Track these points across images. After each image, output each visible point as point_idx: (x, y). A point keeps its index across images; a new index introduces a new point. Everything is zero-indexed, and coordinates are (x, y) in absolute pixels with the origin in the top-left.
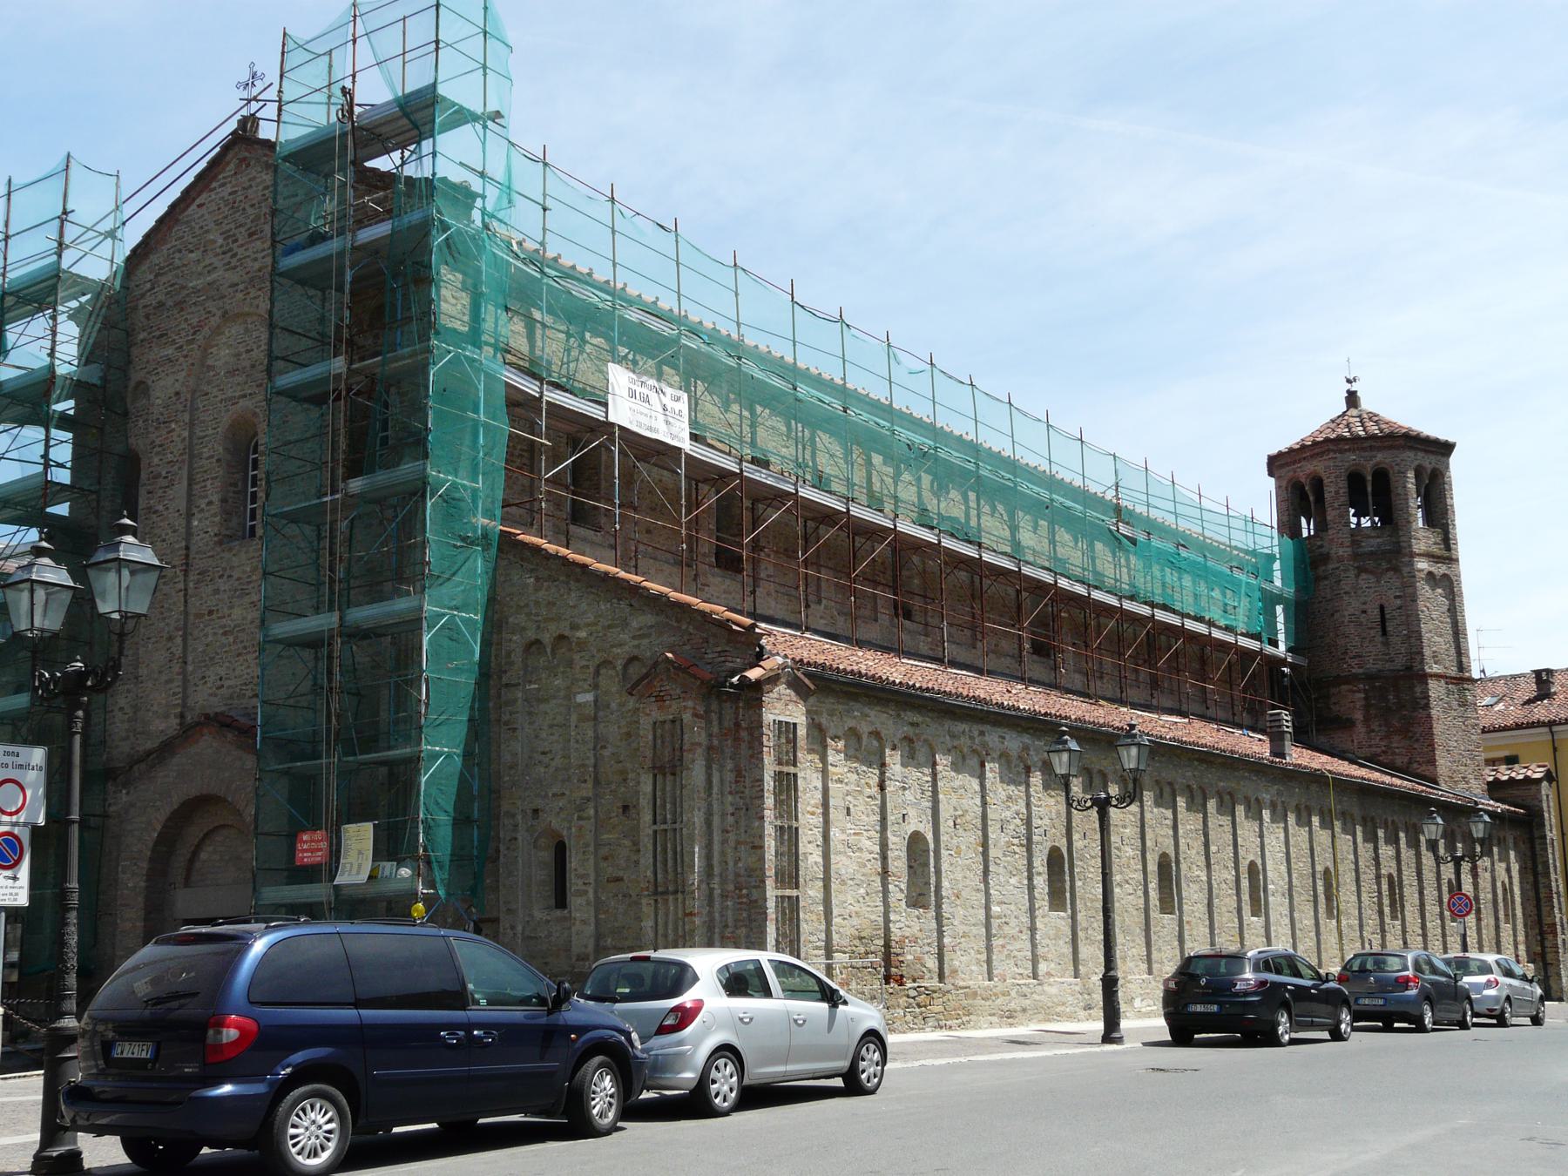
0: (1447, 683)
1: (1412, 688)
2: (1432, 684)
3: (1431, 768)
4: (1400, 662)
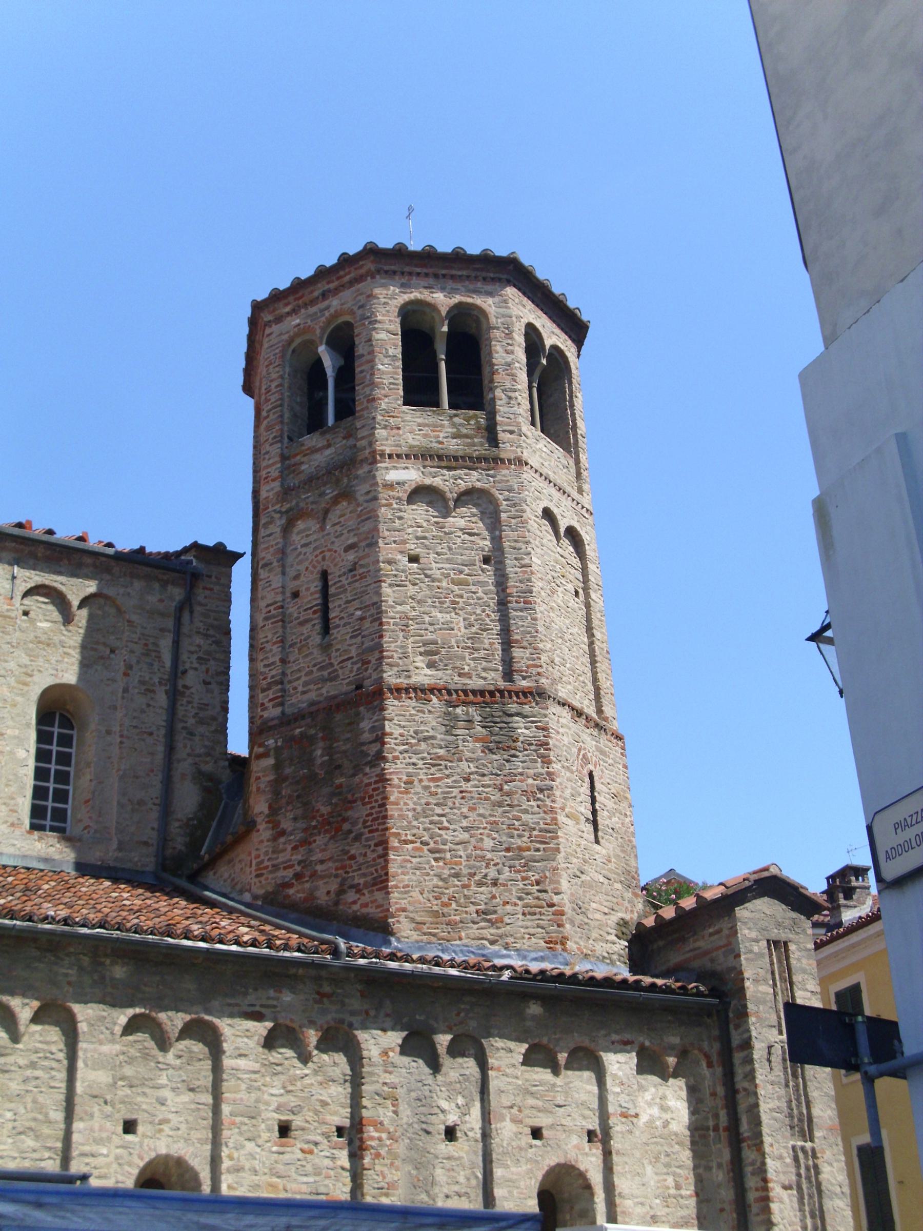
0: (449, 704)
1: (353, 724)
2: (392, 705)
3: (379, 895)
4: (347, 674)
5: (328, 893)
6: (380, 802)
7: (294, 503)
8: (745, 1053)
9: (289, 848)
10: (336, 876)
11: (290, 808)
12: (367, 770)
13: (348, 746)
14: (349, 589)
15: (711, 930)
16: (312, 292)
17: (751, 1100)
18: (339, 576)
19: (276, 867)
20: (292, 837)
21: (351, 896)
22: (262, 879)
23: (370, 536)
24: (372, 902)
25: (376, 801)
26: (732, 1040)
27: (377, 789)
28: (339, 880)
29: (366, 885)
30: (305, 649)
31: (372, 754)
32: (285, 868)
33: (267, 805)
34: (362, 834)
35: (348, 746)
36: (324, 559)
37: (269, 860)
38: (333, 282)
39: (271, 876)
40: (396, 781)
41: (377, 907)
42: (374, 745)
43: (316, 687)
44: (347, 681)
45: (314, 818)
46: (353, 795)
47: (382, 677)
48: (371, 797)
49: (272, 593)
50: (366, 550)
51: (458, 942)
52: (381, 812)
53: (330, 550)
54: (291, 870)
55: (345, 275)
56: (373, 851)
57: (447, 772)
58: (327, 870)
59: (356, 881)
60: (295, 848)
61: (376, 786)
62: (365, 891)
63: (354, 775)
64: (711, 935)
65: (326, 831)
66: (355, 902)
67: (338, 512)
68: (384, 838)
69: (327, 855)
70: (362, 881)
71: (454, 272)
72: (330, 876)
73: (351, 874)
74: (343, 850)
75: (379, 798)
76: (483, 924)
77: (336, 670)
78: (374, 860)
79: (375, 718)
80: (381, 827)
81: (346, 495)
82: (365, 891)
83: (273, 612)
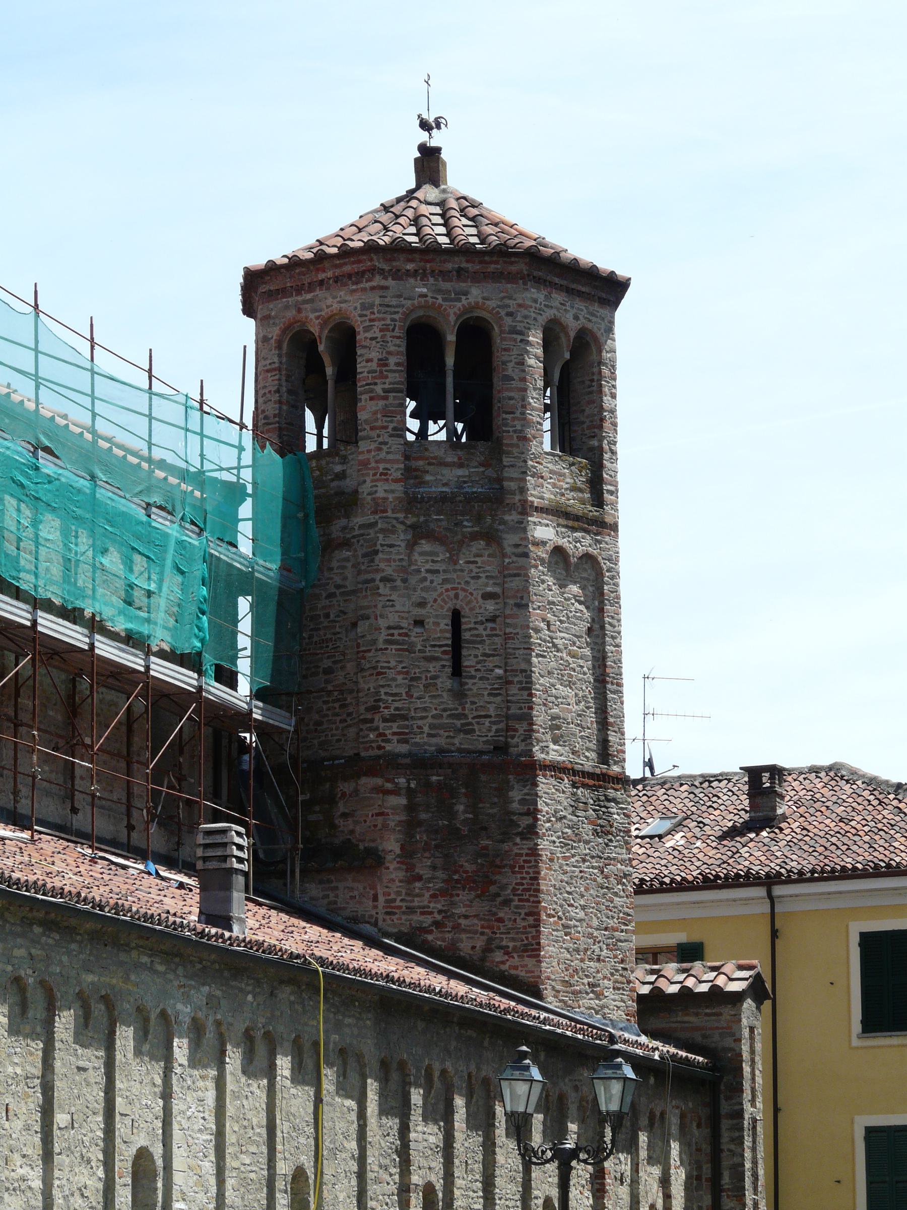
1: (502, 791)
3: (530, 962)
5: (473, 948)
6: (532, 875)
7: (422, 519)
8: (735, 1121)
9: (427, 895)
10: (482, 934)
11: (427, 854)
12: (518, 840)
13: (495, 810)
14: (488, 642)
15: (708, 1011)
16: (445, 261)
17: (736, 1160)
18: (476, 623)
19: (411, 910)
20: (431, 885)
21: (498, 956)
22: (394, 917)
23: (519, 595)
24: (522, 966)
25: (528, 873)
26: (721, 1108)
27: (530, 862)
28: (485, 938)
29: (515, 949)
30: (431, 688)
31: (522, 826)
32: (422, 913)
33: (399, 844)
34: (511, 901)
35: (495, 810)
36: (456, 596)
37: (402, 900)
38: (474, 262)
39: (404, 917)
40: (544, 858)
41: (527, 972)
42: (525, 817)
43: (446, 734)
44: (485, 739)
45: (456, 872)
46: (502, 860)
47: (531, 750)
48: (521, 867)
49: (396, 615)
50: (515, 609)
51: (577, 1010)
52: (532, 884)
53: (464, 590)
54: (429, 917)
55: (491, 263)
56: (524, 919)
57: (573, 851)
58: (473, 925)
59: (504, 943)
60: (433, 896)
61: (528, 858)
62: (515, 955)
63: (503, 842)
64: (707, 1015)
65: (471, 889)
66: (503, 963)
67: (474, 550)
68: (536, 910)
69: (472, 912)
70: (511, 944)
71: (580, 288)
72: (476, 932)
73: (498, 936)
74: (490, 911)
75: (531, 871)
76: (591, 995)
77: (470, 724)
78: (524, 927)
79: (526, 791)
80: (532, 899)
81: (491, 537)
82: (515, 955)
83: (396, 637)
